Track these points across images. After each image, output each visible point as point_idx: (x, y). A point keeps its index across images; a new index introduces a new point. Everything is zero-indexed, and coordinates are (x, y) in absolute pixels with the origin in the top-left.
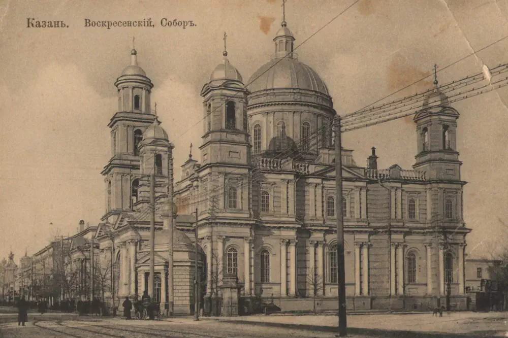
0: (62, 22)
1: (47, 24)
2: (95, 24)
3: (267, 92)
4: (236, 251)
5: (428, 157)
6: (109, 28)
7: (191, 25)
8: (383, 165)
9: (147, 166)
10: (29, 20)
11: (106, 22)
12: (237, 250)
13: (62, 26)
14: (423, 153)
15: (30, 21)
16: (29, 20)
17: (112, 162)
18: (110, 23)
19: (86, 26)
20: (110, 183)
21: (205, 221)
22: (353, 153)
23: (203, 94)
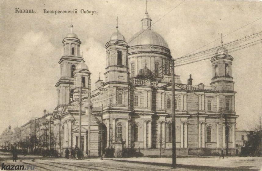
1: (25, 11)
2: (48, 12)
5: (218, 79)
6: (56, 14)
8: (195, 84)
9: (78, 83)
10: (16, 9)
14: (216, 77)
15: (17, 9)
16: (16, 9)
18: (56, 12)
19: (44, 13)
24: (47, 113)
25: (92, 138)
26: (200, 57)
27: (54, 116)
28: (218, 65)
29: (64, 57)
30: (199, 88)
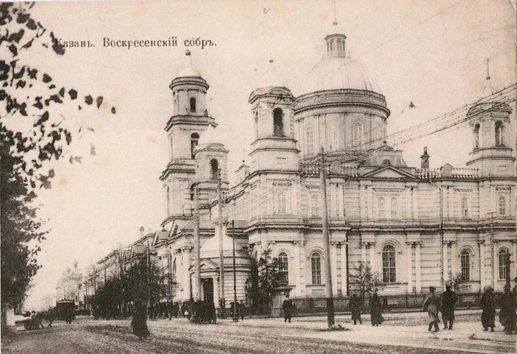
0: (89, 42)
3: (318, 94)
4: (286, 255)
7: (210, 45)
8: (435, 164)
9: (204, 172)
11: (126, 42)
12: (287, 254)
13: (89, 46)
14: (477, 149)
17: (170, 168)
19: (104, 45)
20: (168, 188)
21: (254, 228)
22: (403, 153)
23: (251, 101)
24: (145, 233)
25: (230, 292)
26: (398, 187)
27: (156, 241)
28: (481, 124)
29: (175, 119)
30: (443, 174)
